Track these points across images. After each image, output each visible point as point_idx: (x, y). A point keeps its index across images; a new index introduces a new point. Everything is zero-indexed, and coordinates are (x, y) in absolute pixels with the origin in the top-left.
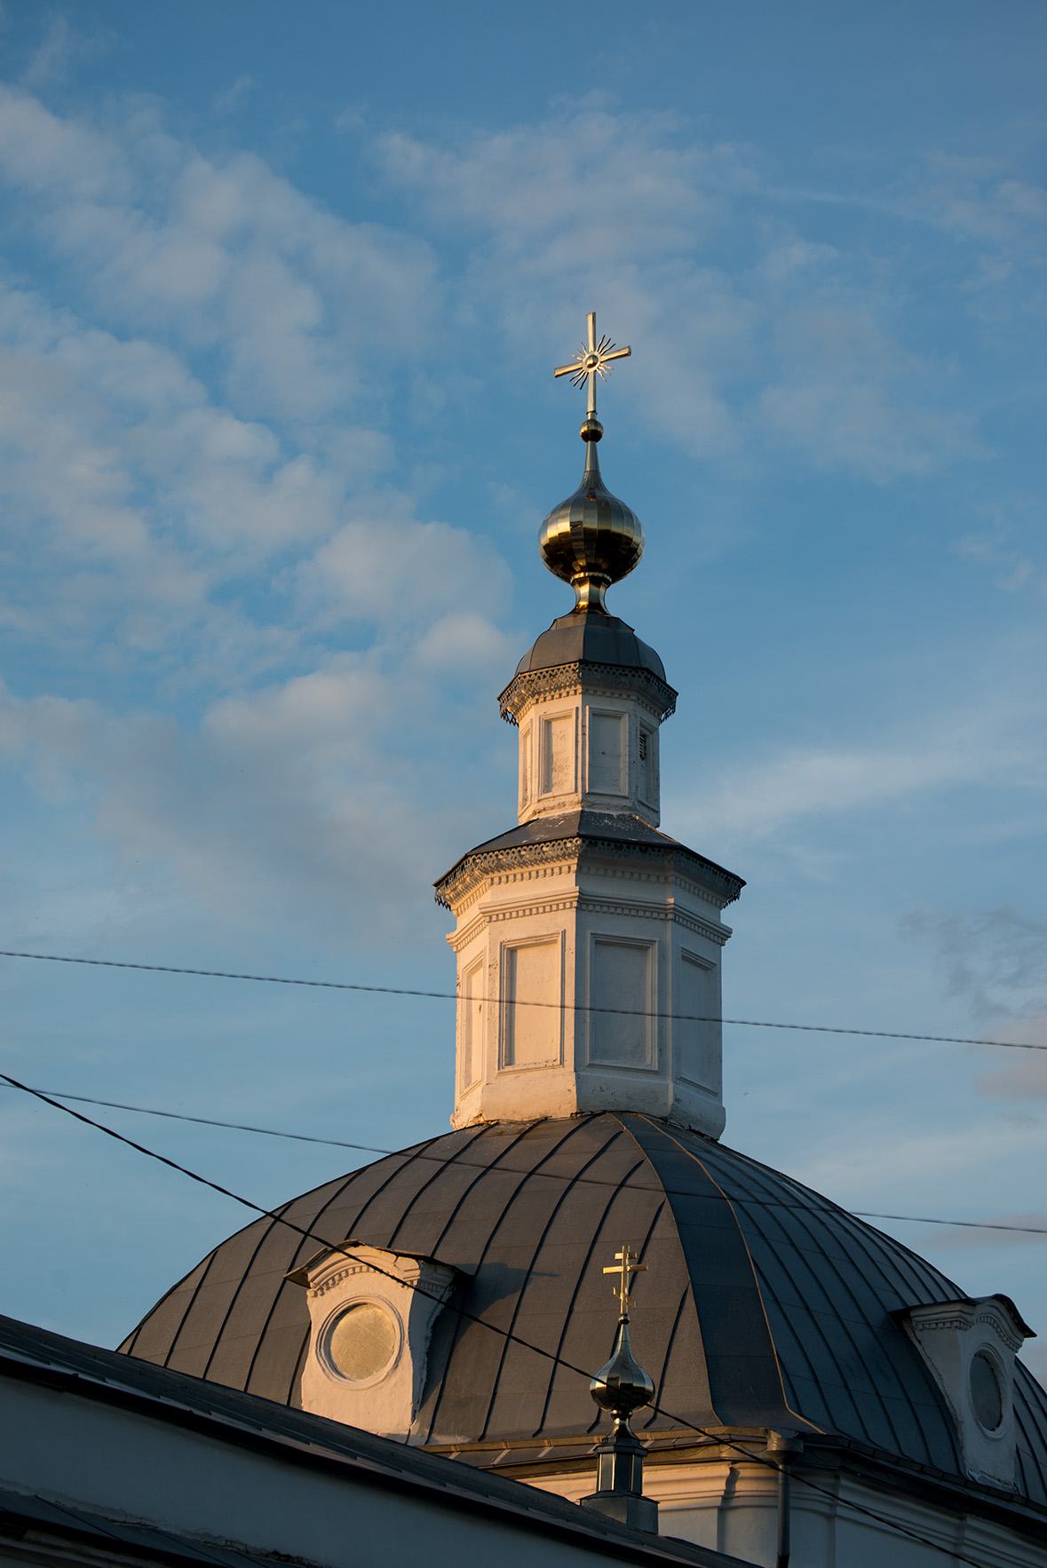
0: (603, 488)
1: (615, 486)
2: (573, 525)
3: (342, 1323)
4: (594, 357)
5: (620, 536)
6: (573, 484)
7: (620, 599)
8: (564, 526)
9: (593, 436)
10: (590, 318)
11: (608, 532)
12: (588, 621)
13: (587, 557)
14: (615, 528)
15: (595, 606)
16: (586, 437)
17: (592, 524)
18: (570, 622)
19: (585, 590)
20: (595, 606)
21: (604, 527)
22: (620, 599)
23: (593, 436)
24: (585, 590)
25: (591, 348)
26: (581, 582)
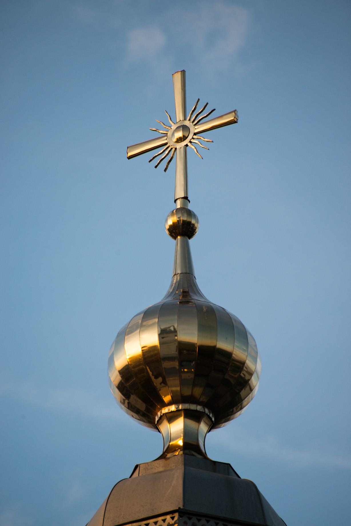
0: (197, 292)
1: (212, 290)
2: (163, 334)
3: (162, 151)
4: (185, 128)
5: (228, 355)
6: (160, 288)
7: (221, 443)
8: (150, 338)
9: (184, 230)
10: (178, 77)
11: (214, 347)
12: (186, 464)
13: (183, 383)
14: (223, 345)
15: (192, 448)
16: (175, 231)
17: (190, 335)
18: (160, 466)
19: (178, 426)
20: (192, 448)
21: (208, 342)
22: (221, 443)
23: (184, 230)
24: (178, 426)
25: (180, 116)
26: (171, 417)
